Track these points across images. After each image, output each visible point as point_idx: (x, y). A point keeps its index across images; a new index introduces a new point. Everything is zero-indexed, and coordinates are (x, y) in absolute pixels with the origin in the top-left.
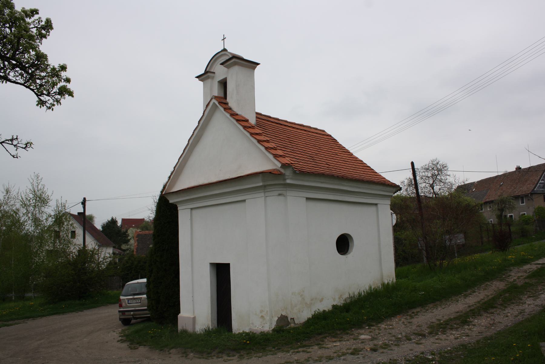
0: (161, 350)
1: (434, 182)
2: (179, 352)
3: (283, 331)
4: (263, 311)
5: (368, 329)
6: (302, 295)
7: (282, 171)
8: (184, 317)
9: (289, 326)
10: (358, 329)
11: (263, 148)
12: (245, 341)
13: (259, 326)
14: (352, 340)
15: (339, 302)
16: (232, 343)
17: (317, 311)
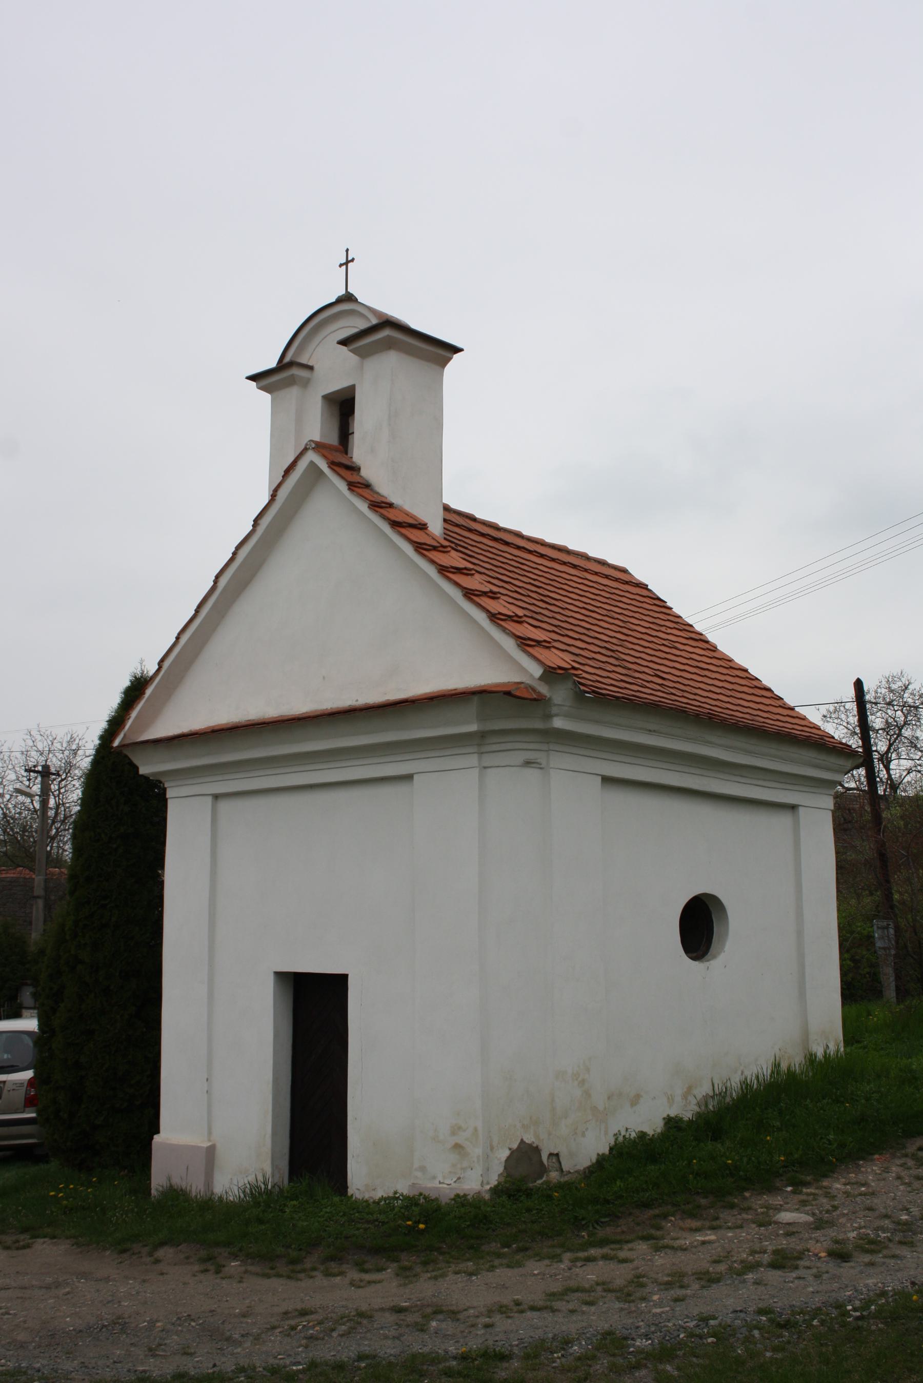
0: (124, 1251)
1: (890, 745)
2: (188, 1258)
3: (529, 1193)
4: (460, 1128)
5: (793, 1192)
6: (583, 1081)
7: (544, 689)
8: (175, 1149)
9: (544, 1179)
10: (764, 1194)
11: (481, 617)
12: (409, 1223)
13: (444, 1177)
14: (754, 1226)
15: (686, 1111)
16: (366, 1229)
17: (623, 1133)
